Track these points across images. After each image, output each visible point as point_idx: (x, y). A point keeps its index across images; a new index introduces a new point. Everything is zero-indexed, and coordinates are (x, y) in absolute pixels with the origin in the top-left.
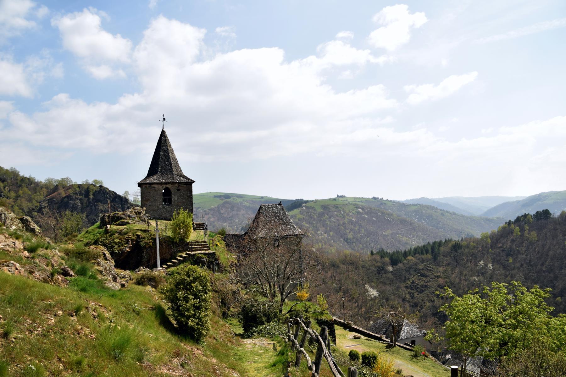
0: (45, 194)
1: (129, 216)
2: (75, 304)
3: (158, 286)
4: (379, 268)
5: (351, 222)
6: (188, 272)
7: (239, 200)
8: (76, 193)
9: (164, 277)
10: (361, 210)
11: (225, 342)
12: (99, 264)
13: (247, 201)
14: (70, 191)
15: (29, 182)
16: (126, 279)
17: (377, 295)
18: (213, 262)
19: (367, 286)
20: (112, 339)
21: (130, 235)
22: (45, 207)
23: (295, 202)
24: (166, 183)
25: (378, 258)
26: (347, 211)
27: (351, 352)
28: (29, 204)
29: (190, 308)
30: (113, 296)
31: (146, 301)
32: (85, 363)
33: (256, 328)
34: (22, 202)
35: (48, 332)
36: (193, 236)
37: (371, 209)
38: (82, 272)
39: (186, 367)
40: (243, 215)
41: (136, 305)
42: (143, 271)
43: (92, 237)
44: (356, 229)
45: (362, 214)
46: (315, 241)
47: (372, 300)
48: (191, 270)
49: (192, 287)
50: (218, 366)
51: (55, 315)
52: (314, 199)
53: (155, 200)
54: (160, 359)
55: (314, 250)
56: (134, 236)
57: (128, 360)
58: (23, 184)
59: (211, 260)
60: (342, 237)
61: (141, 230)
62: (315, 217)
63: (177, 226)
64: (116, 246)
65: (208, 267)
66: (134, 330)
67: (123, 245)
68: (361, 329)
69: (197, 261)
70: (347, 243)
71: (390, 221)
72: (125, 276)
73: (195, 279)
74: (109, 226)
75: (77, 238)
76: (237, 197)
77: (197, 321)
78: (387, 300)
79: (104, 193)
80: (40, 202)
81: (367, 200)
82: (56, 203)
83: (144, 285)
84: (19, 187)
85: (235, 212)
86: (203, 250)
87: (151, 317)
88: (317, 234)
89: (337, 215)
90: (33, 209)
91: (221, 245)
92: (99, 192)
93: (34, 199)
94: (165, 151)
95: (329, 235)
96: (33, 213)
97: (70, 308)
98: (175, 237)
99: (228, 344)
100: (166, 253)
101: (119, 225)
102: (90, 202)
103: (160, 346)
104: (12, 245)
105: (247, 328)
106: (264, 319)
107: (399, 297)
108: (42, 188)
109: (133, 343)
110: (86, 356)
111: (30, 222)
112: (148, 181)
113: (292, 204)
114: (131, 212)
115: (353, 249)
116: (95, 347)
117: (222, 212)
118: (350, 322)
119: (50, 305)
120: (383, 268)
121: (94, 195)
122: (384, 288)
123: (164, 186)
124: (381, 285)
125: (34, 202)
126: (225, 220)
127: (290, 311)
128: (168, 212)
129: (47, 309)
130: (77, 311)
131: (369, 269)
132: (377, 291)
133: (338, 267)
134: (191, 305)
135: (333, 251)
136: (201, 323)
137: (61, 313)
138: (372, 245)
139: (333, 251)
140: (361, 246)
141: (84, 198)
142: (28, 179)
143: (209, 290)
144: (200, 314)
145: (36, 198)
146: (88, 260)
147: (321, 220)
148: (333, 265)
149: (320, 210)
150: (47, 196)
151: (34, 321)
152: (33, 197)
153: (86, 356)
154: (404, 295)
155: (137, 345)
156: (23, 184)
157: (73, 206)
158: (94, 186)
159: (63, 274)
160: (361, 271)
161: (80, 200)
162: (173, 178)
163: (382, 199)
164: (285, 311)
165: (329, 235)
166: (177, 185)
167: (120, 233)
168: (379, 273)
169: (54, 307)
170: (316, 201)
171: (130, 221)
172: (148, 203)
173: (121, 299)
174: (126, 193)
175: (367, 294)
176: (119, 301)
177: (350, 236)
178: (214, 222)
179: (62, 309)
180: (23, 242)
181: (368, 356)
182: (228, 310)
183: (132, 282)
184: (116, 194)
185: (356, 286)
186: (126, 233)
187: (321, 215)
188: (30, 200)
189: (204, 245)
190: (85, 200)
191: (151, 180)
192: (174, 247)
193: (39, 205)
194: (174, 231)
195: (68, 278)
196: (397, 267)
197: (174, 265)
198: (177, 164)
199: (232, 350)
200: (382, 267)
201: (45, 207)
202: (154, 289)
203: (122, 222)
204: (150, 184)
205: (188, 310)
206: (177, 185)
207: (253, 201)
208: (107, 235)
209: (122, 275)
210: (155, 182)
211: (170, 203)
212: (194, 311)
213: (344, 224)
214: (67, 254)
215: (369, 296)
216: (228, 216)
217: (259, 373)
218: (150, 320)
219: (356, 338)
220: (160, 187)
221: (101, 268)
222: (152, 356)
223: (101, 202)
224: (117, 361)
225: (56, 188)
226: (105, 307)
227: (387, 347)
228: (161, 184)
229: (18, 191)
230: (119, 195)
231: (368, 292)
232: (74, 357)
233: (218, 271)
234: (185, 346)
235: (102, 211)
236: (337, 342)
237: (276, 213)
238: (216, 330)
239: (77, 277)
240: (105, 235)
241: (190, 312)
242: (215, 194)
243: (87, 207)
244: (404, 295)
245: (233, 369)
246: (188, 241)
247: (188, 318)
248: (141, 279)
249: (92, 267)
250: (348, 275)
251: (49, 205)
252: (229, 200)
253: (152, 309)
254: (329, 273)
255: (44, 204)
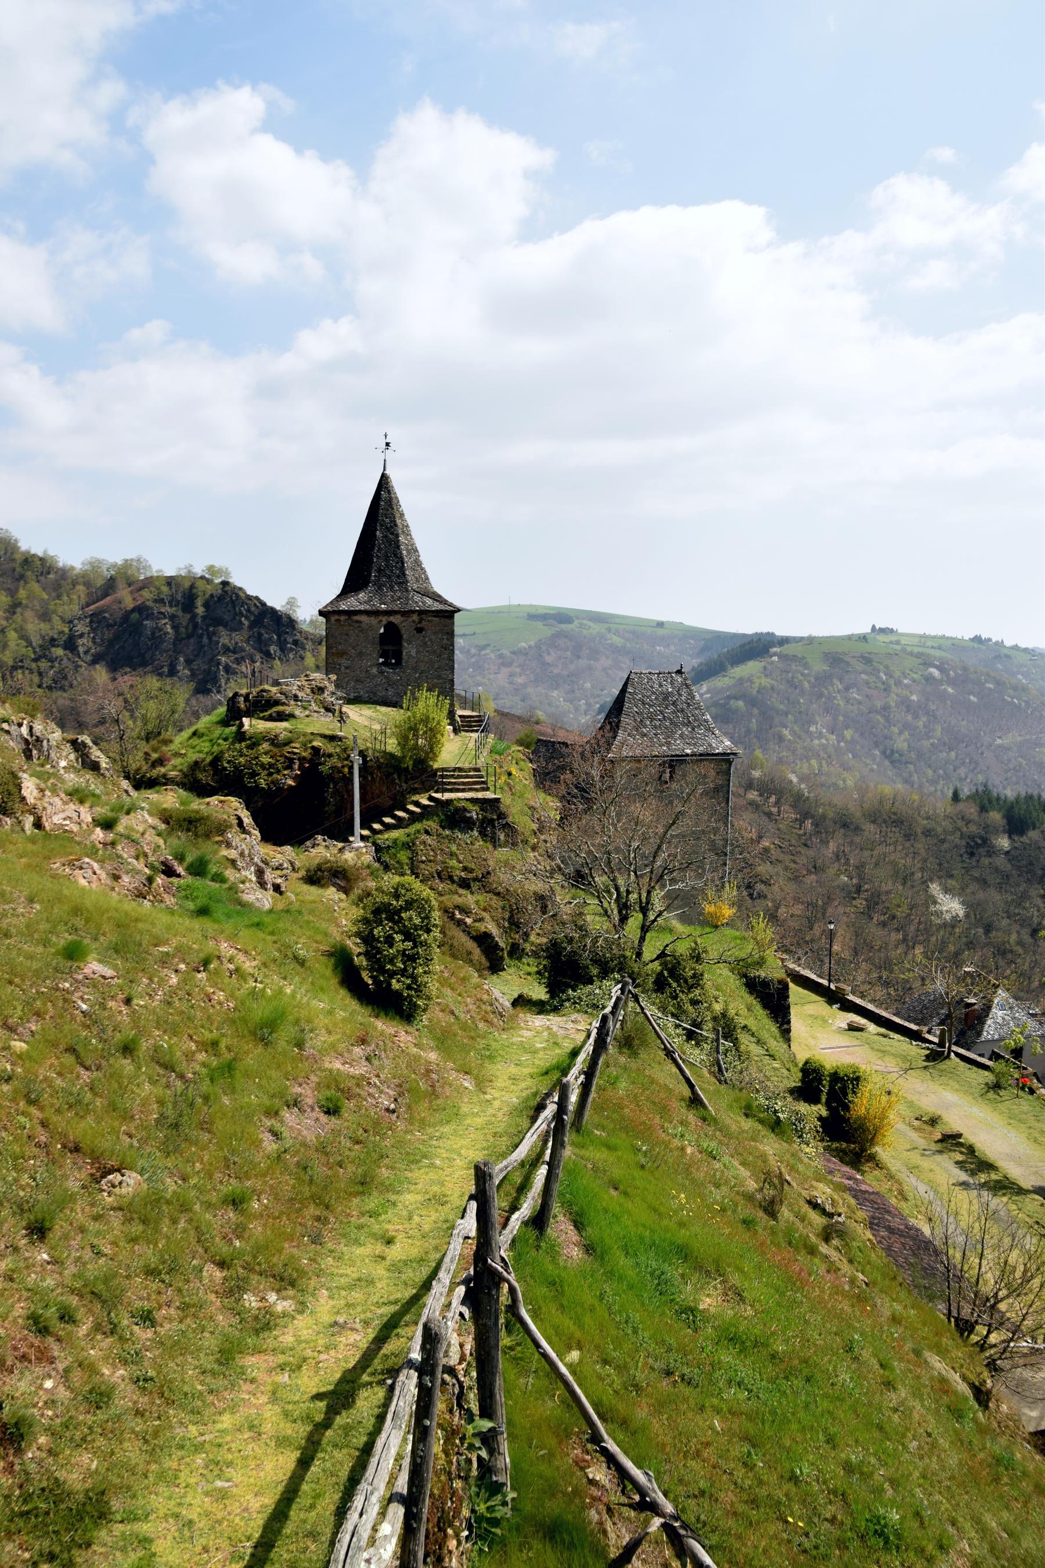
0: (83, 601)
1: (296, 698)
2: (200, 950)
3: (351, 888)
4: (972, 838)
5: (906, 704)
6: (396, 890)
7: (596, 628)
8: (161, 601)
9: (368, 867)
10: (936, 673)
11: (473, 1022)
12: (229, 845)
13: (617, 633)
14: (146, 594)
15: (40, 568)
16: (285, 872)
17: (961, 913)
18: (493, 820)
19: (935, 888)
20: (259, 1012)
21: (297, 747)
22: (81, 636)
23: (751, 642)
24: (390, 615)
25: (971, 810)
26: (897, 674)
27: (806, 1063)
28: (42, 625)
29: (395, 957)
30: (258, 924)
31: (319, 937)
32: (222, 1045)
33: (574, 990)
34: (25, 621)
35: (172, 997)
36: (452, 751)
37: (965, 669)
38: (198, 869)
39: (376, 1062)
40: (604, 669)
41: (299, 946)
42: (322, 850)
43: (206, 746)
44: (921, 723)
45: (940, 682)
46: (799, 752)
47: (945, 925)
48: (403, 885)
49: (402, 918)
50: (438, 1065)
51: (176, 971)
52: (805, 635)
53: (360, 654)
54: (333, 1046)
55: (795, 780)
56: (305, 750)
57: (282, 1045)
58: (29, 573)
59: (489, 816)
60: (876, 745)
61: (324, 736)
62: (806, 685)
63: (410, 728)
64: (264, 773)
65: (480, 833)
66: (293, 996)
67: (278, 772)
68: (870, 1007)
69: (454, 818)
70: (892, 762)
71: (1018, 707)
72: (281, 865)
73: (409, 905)
74: (246, 721)
75: (172, 747)
76: (590, 620)
77: (409, 981)
78: (988, 929)
79: (233, 602)
80: (71, 622)
81: (955, 645)
82: (109, 626)
83: (322, 886)
84: (18, 580)
85: (583, 663)
86: (471, 790)
87: (325, 971)
88: (808, 732)
89: (867, 683)
90: (53, 640)
91: (523, 773)
92: (221, 599)
93: (55, 612)
94: (388, 529)
95: (841, 738)
96: (53, 649)
97: (195, 959)
98: (404, 757)
99: (481, 1025)
100: (382, 793)
101: (270, 719)
102: (196, 626)
103: (335, 1025)
104: (75, 815)
105: (555, 988)
106: (595, 971)
107: (1023, 922)
108: (74, 584)
109: (291, 1018)
110: (223, 1035)
111: (90, 748)
112: (343, 607)
113: (742, 646)
114: (301, 688)
115: (906, 781)
116: (233, 1022)
117: (548, 659)
118: (845, 987)
119: (167, 953)
120: (985, 841)
121: (206, 605)
122: (981, 895)
123: (385, 620)
124: (973, 887)
125: (55, 619)
126: (555, 682)
127: (662, 955)
128: (390, 683)
129: (165, 960)
130: (206, 963)
131: (943, 841)
132: (963, 903)
133: (858, 829)
134: (398, 951)
135: (850, 783)
136: (416, 986)
137: (182, 966)
138: (962, 771)
139: (850, 783)
140: (930, 772)
141: (180, 613)
142: (41, 559)
143: (435, 926)
144: (414, 968)
145: (60, 610)
146: (207, 836)
147: (821, 695)
148: (845, 824)
149: (820, 667)
150: (88, 605)
151: (151, 980)
152: (52, 607)
153: (223, 1035)
154: (1036, 920)
155: (297, 1022)
156: (29, 573)
157: (153, 633)
158: (209, 581)
159: (164, 872)
160: (921, 846)
161: (172, 618)
162: (407, 599)
163: (1000, 644)
164: (649, 952)
165: (841, 738)
166: (415, 617)
167: (274, 741)
168: (972, 854)
169: (174, 956)
170: (810, 640)
171: (297, 712)
172: (344, 662)
173: (272, 933)
174: (292, 602)
175: (932, 908)
176: (269, 938)
177: (901, 743)
178: (525, 686)
179: (184, 961)
180: (91, 807)
181: (842, 1075)
182: (525, 941)
183: (296, 875)
184: (264, 604)
185: (904, 884)
186: (288, 743)
187: (823, 680)
188: (45, 616)
189: (476, 778)
190: (184, 619)
191: (352, 603)
192: (399, 779)
193: (66, 630)
194: (403, 741)
195: (174, 880)
196: (1024, 839)
197: (400, 823)
198: (418, 563)
199: (484, 1038)
200: (982, 838)
201: (81, 636)
202: (343, 896)
203: (278, 713)
204: (350, 613)
205: (391, 961)
206: (415, 617)
207: (633, 633)
208: (243, 744)
209: (274, 863)
210: (362, 607)
211: (399, 663)
212: (404, 963)
213: (886, 708)
214: (166, 821)
215: (939, 914)
216: (565, 673)
217: (513, 1084)
218: (323, 976)
219: (852, 1028)
220: (373, 620)
221: (233, 854)
222: (318, 1040)
223: (225, 626)
224: (266, 1044)
225: (110, 585)
226: (246, 952)
227: (928, 1058)
228: (377, 613)
229: (17, 590)
230: (272, 608)
231: (935, 902)
232: (208, 1036)
233: (505, 844)
234: (384, 1027)
235: (227, 650)
236: (793, 1034)
237: (666, 696)
238: (460, 995)
239: (190, 880)
240: (237, 746)
241: (394, 965)
242: (532, 611)
243: (189, 637)
244: (1036, 920)
245: (466, 1073)
246: (436, 766)
247: (392, 974)
248: (316, 872)
249: (216, 852)
250: (885, 854)
251: (94, 630)
252: (570, 626)
253: (330, 954)
254: (832, 845)
255: (81, 627)
